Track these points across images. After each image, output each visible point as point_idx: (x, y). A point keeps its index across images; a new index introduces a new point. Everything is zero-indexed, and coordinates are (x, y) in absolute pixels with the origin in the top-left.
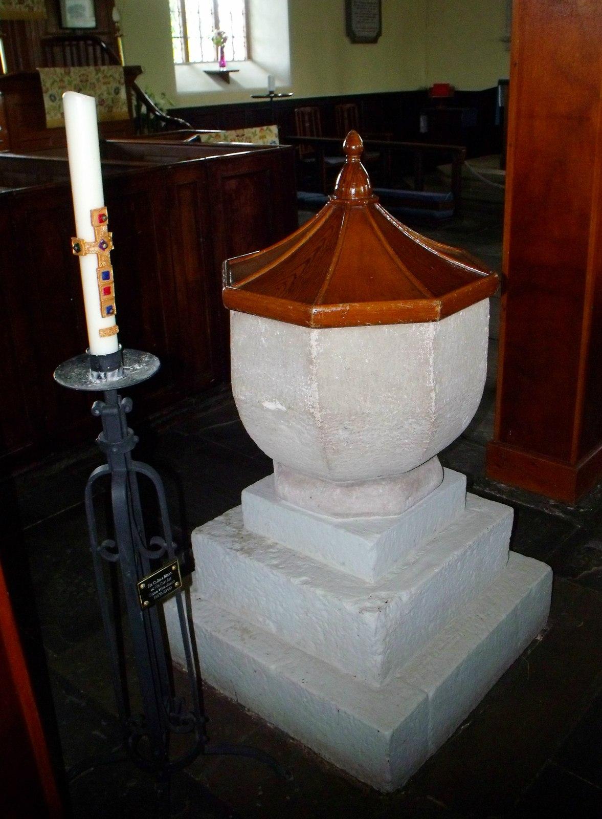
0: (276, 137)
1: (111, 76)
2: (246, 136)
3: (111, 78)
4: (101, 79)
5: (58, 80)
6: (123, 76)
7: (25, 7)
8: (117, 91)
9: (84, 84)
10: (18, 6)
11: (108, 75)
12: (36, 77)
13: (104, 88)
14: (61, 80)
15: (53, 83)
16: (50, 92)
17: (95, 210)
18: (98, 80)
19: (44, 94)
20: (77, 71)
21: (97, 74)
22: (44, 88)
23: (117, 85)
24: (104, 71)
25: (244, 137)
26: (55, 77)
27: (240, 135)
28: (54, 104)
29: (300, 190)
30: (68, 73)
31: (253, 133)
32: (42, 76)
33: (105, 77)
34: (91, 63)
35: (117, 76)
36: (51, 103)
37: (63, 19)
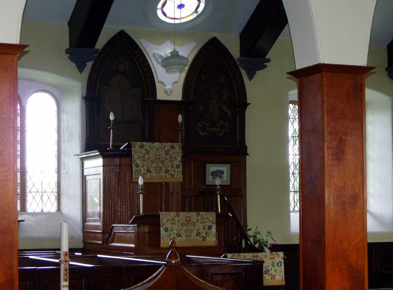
0: (282, 259)
1: (207, 218)
3: (207, 220)
4: (200, 220)
5: (171, 219)
7: (169, 175)
8: (210, 228)
10: (164, 174)
11: (205, 218)
12: (158, 216)
13: (201, 225)
14: (173, 220)
15: (168, 221)
16: (165, 226)
18: (198, 220)
19: (161, 227)
20: (184, 214)
23: (211, 224)
24: (202, 215)
25: (258, 257)
26: (169, 218)
27: (255, 256)
28: (167, 233)
30: (178, 216)
31: (265, 255)
32: (161, 217)
33: (203, 218)
34: (95, 217)
35: (211, 218)
36: (165, 233)
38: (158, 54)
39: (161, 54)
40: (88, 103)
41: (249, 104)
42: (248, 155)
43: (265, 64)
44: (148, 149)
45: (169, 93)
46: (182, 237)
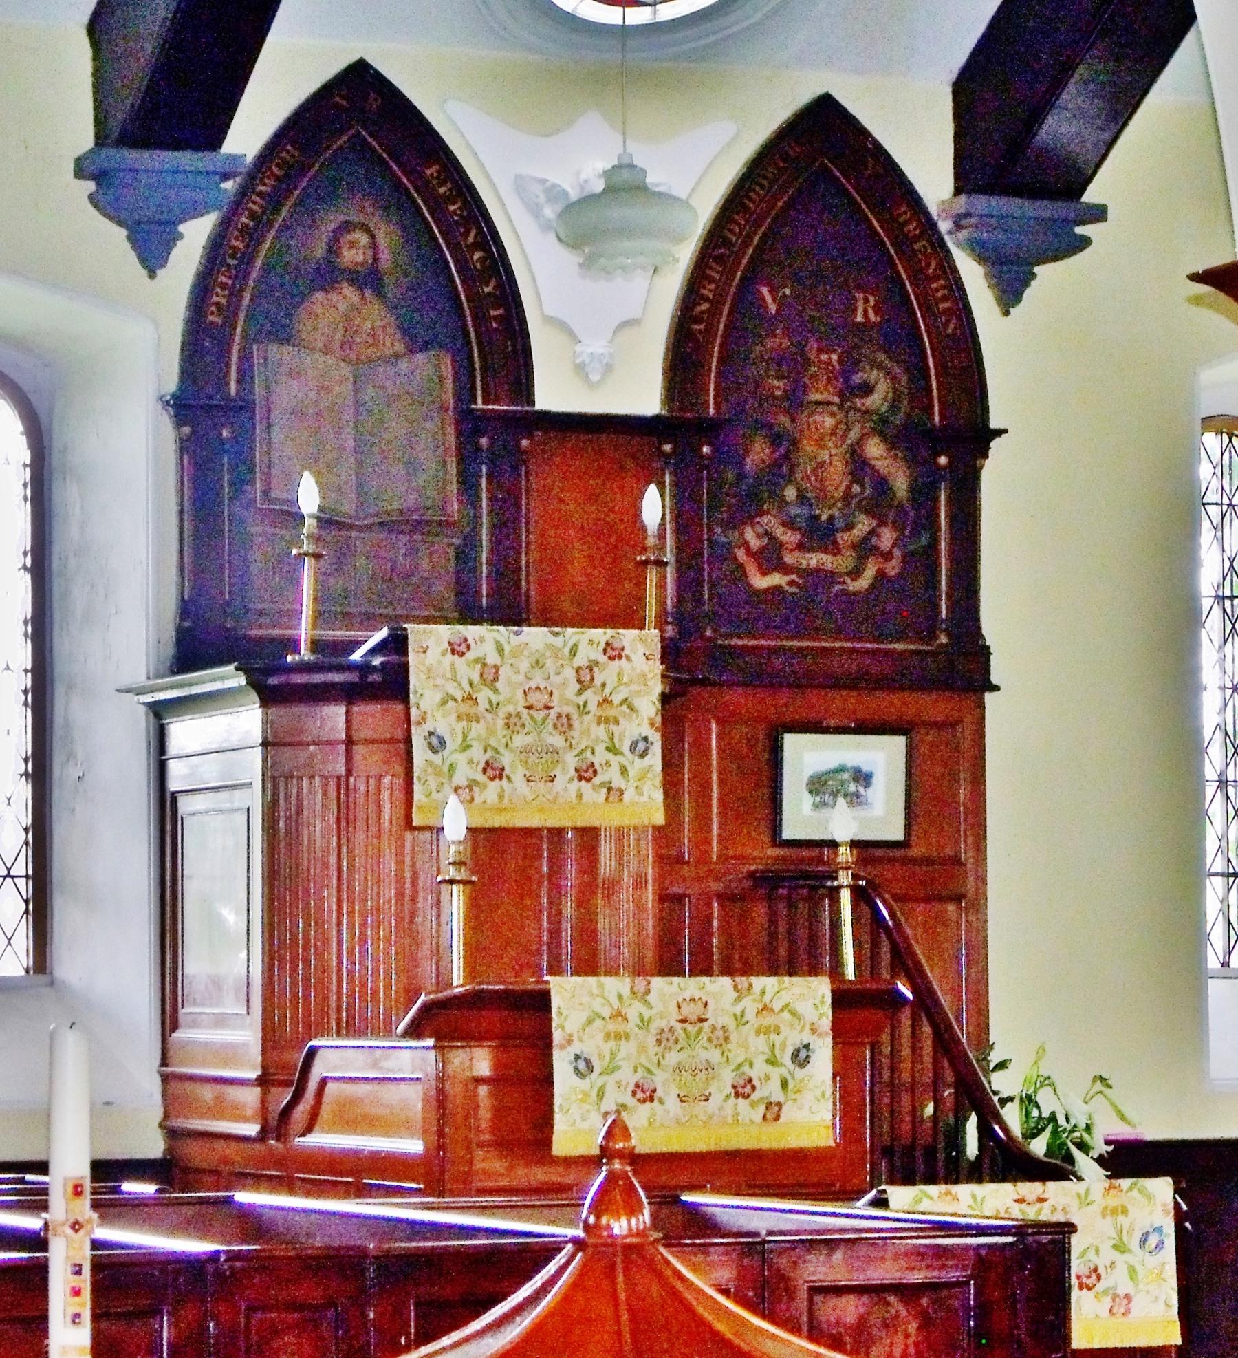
2: (1051, 1202)
3: (786, 1015)
5: (459, 695)
6: (827, 1010)
8: (801, 1057)
9: (692, 1029)
11: (777, 1006)
12: (541, 1001)
17: (70, 1179)
18: (740, 1019)
21: (738, 999)
22: (557, 1036)
23: (806, 1037)
29: (1066, 1338)
31: (1079, 1195)
37: (47, 593)
38: (543, 181)
39: (553, 179)
40: (186, 430)
41: (1000, 432)
42: (996, 688)
43: (1079, 230)
44: (493, 659)
45: (595, 377)
46: (661, 1102)
